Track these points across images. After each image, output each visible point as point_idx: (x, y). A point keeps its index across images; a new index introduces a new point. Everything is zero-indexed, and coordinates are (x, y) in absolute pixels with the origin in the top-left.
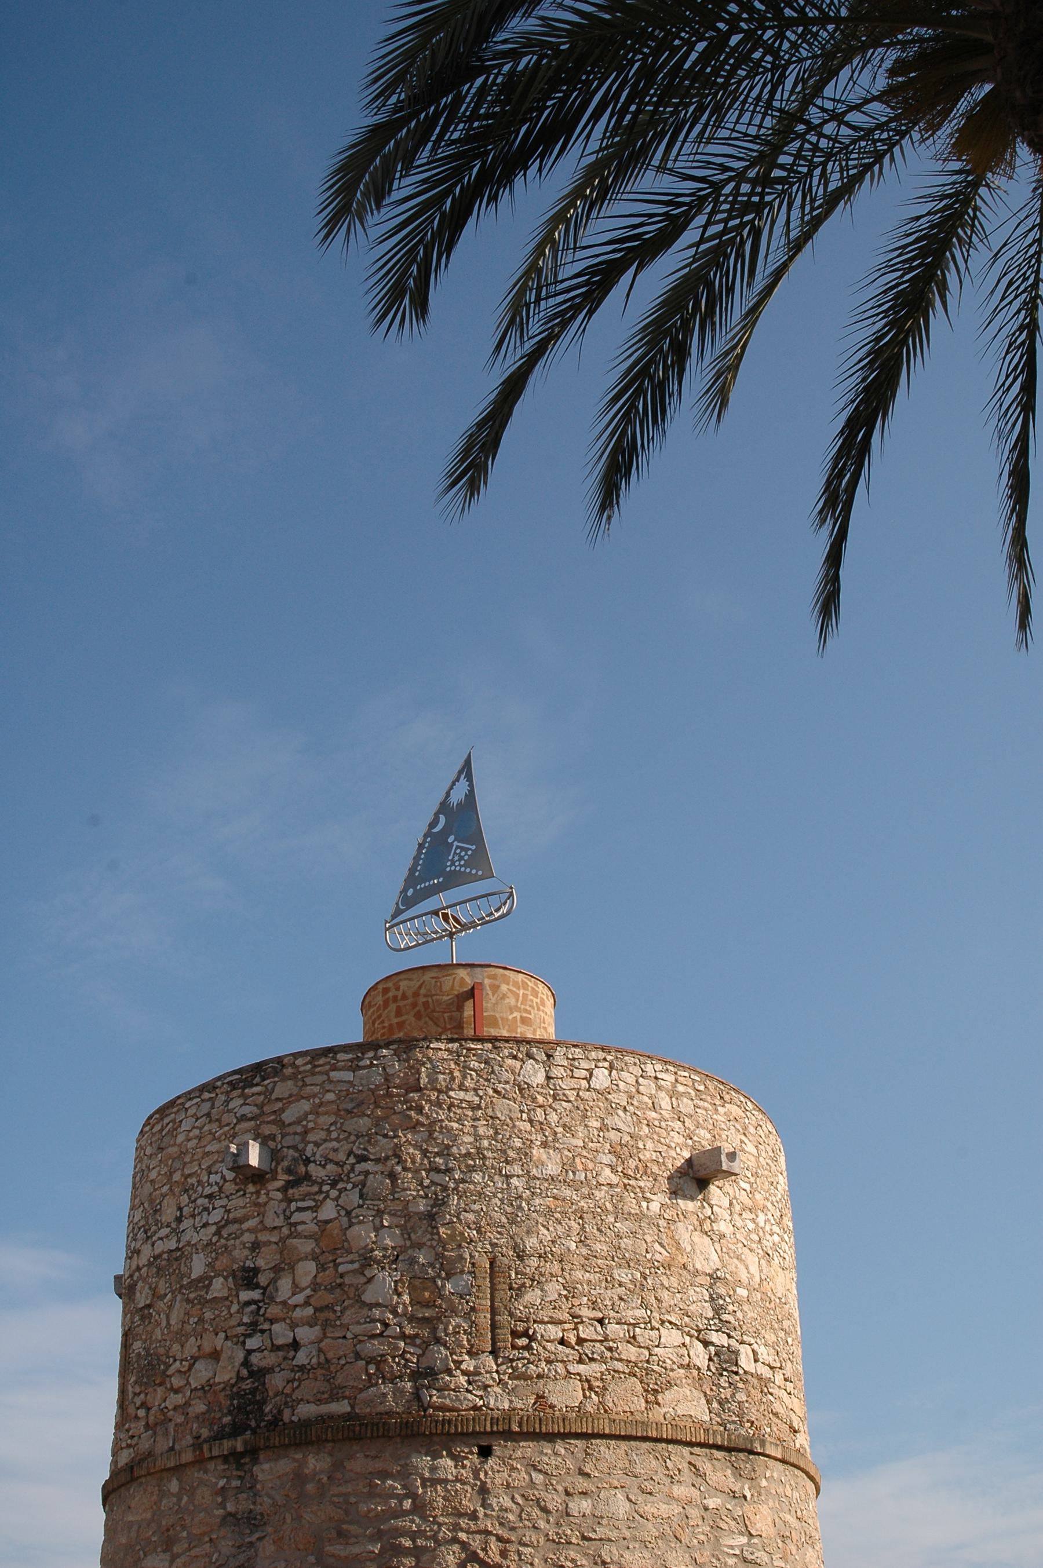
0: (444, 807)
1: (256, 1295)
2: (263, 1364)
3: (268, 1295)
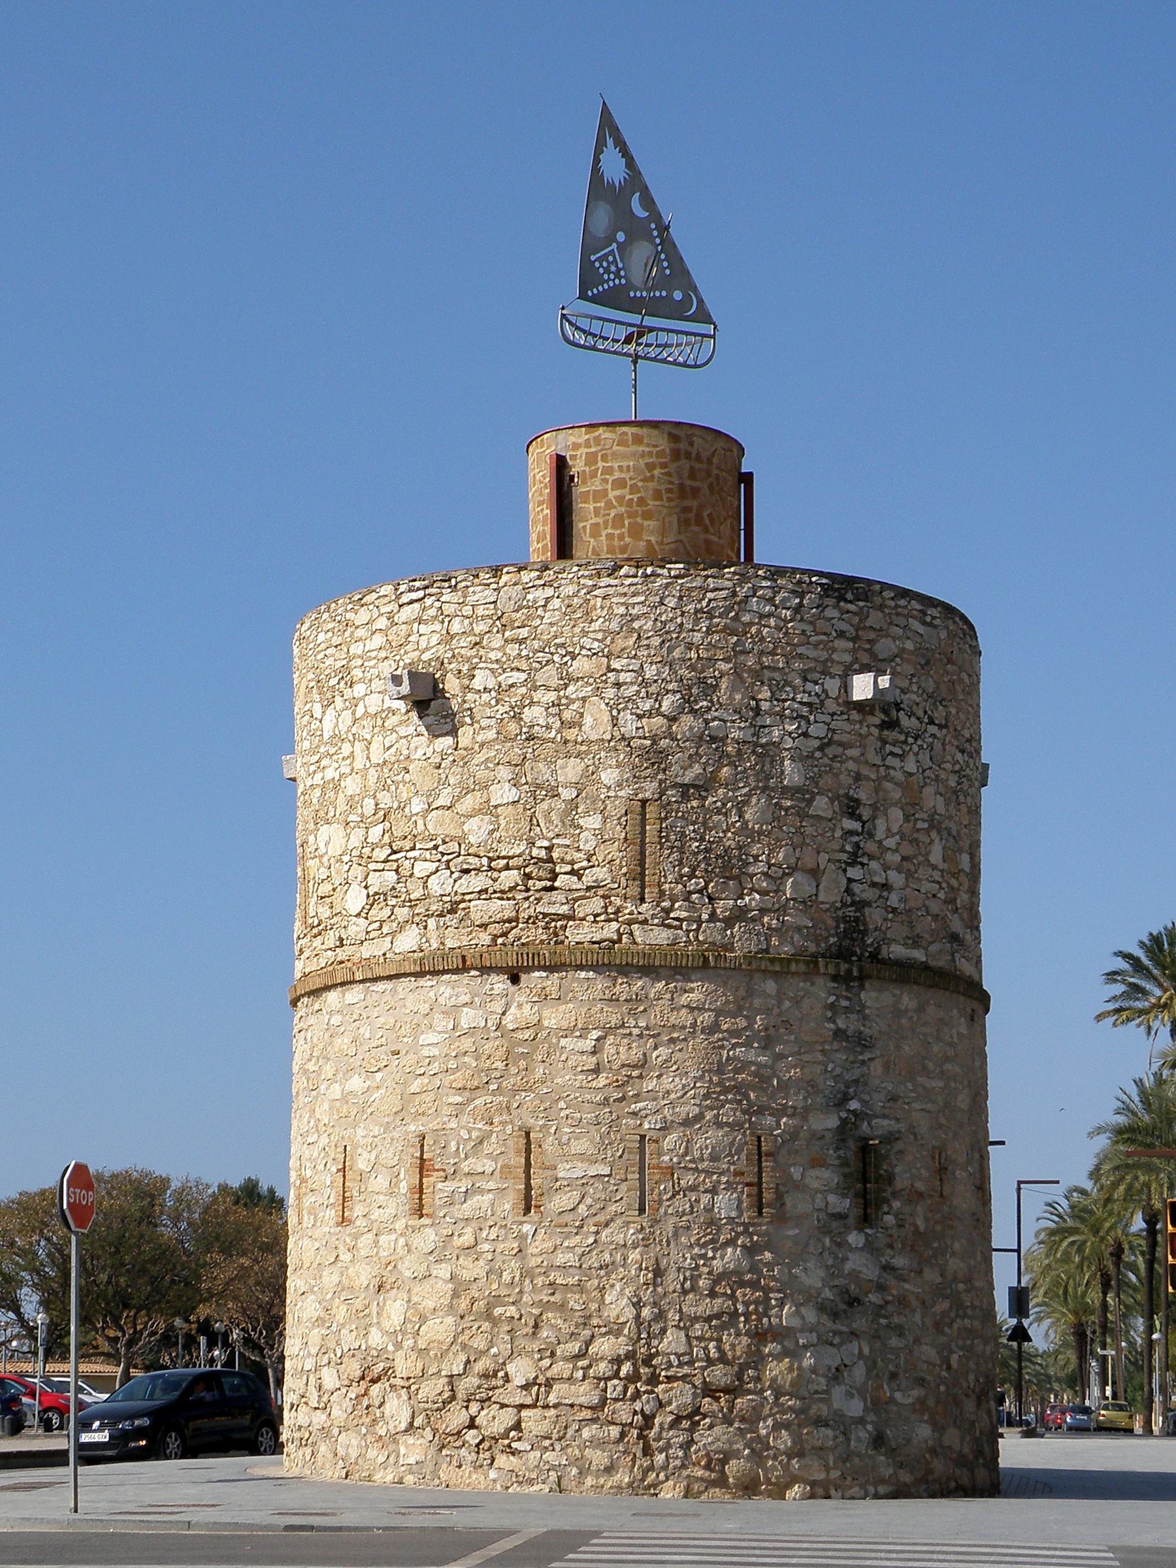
1: (857, 826)
2: (865, 896)
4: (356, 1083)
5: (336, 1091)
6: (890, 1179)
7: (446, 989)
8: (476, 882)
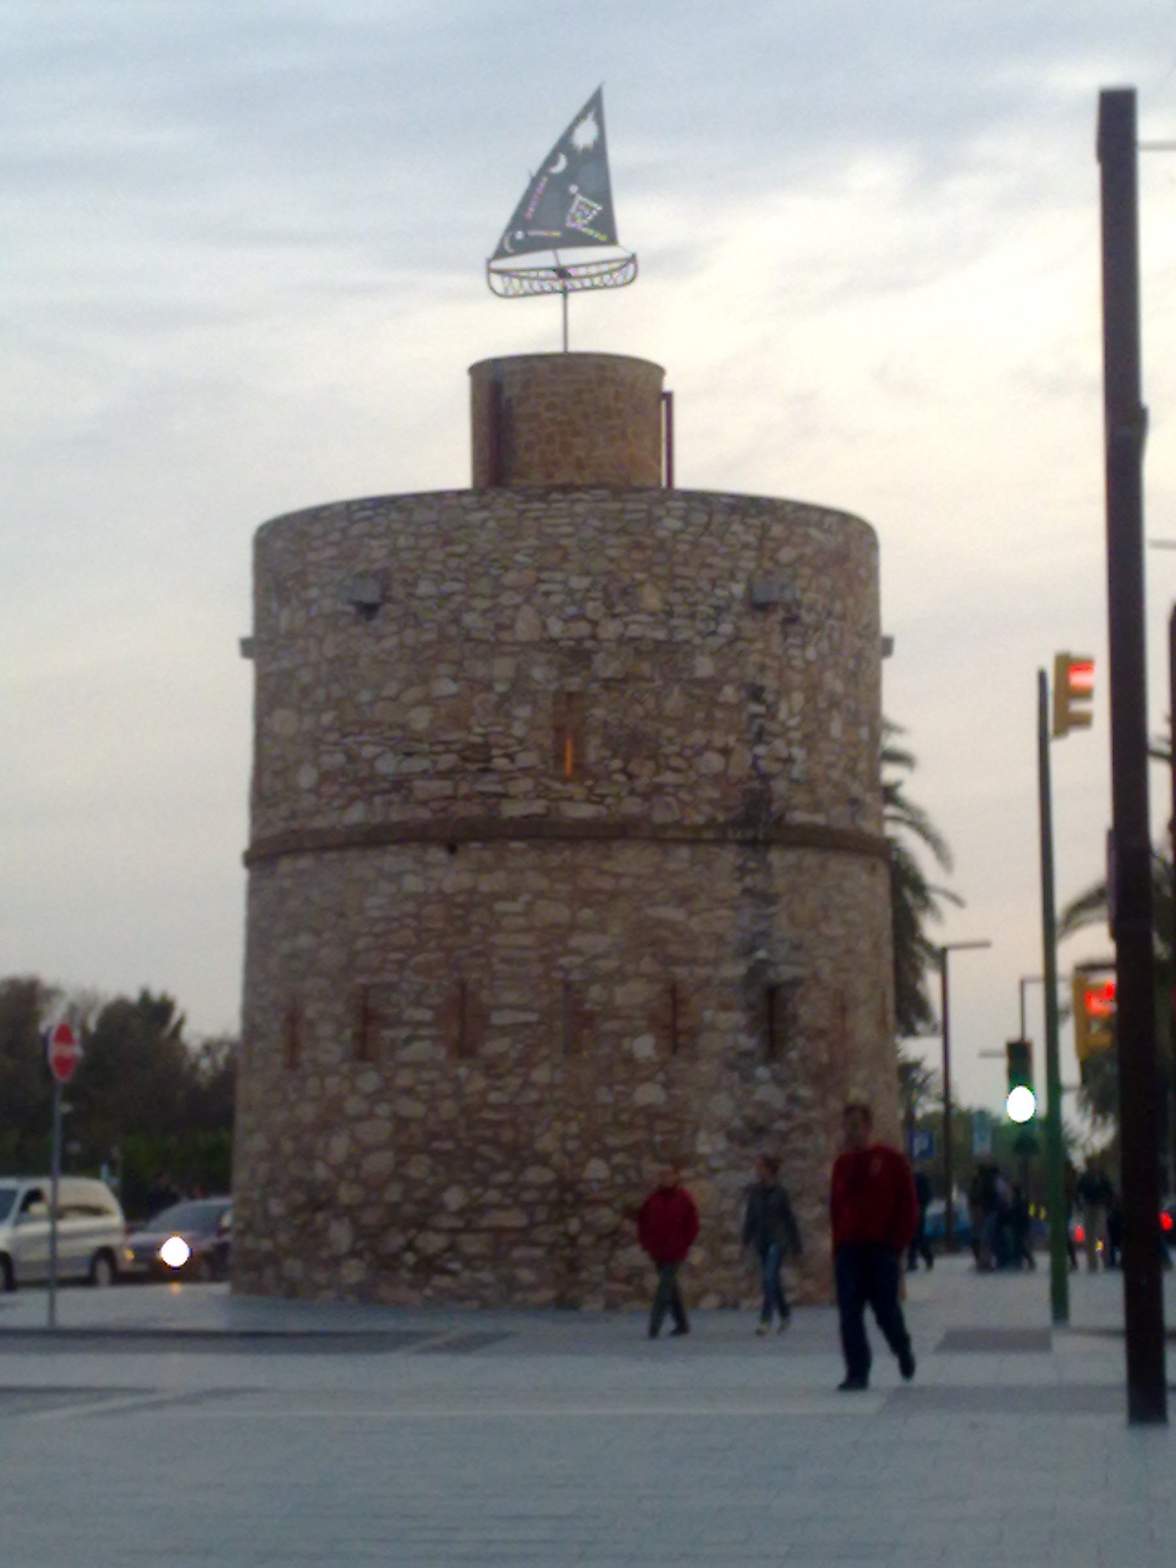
0: (564, 145)
3: (772, 714)
4: (305, 941)
5: (285, 947)
6: (795, 1018)
7: (391, 860)
8: (418, 764)
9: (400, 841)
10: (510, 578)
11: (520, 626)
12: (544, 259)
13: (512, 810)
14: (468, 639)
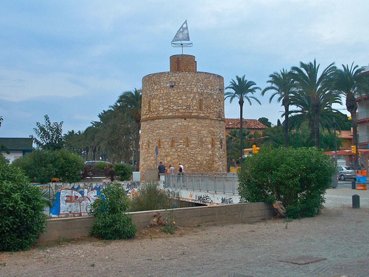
7: (176, 120)
8: (180, 108)
9: (177, 118)
10: (193, 83)
11: (194, 90)
12: (179, 42)
13: (193, 114)
14: (187, 91)
